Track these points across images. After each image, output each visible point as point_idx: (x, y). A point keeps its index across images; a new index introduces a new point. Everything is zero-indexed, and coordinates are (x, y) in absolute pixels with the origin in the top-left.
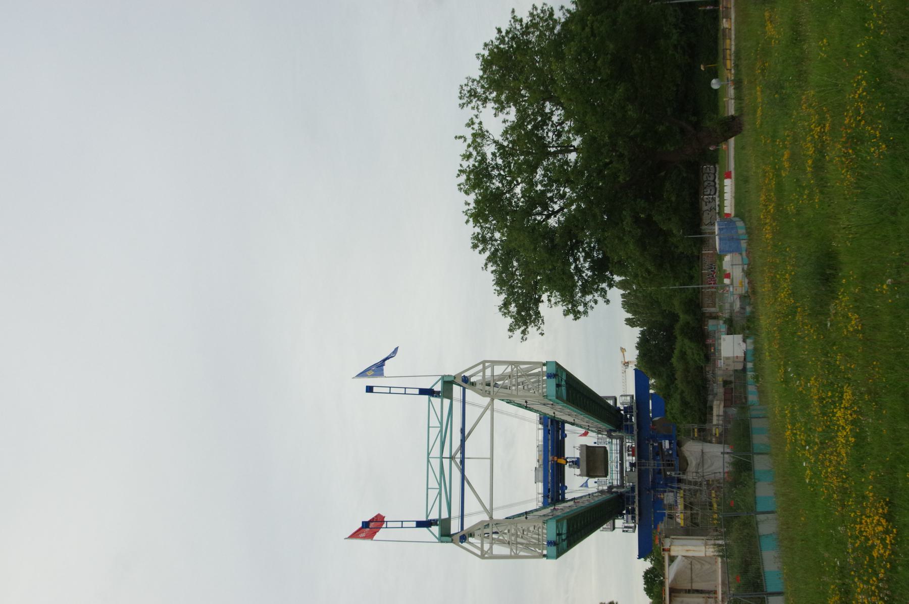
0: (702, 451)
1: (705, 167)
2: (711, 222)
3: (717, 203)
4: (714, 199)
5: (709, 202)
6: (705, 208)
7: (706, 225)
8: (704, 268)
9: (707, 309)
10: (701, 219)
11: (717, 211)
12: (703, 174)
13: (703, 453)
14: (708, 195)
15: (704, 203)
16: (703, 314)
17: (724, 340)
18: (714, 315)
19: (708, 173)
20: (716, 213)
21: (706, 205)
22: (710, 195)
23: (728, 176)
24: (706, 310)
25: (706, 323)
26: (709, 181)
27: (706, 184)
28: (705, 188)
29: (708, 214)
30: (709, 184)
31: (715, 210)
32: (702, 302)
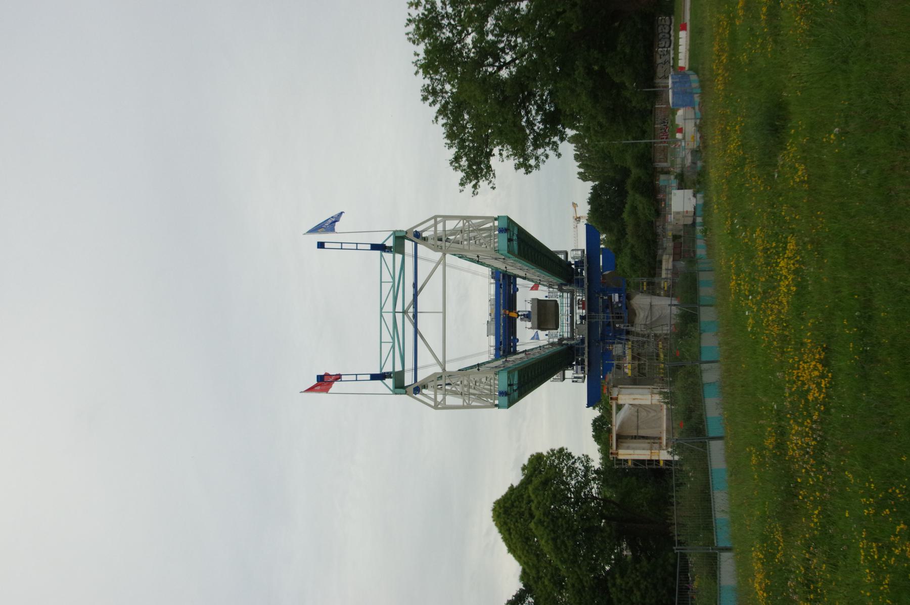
0: (651, 304)
1: (660, 18)
2: (665, 76)
3: (672, 56)
4: (668, 52)
5: (664, 55)
6: (659, 61)
7: (661, 78)
8: (657, 122)
9: (659, 164)
10: (655, 73)
11: (671, 64)
12: (658, 26)
13: (651, 305)
14: (662, 48)
15: (658, 56)
16: (655, 168)
17: (675, 194)
18: (665, 170)
19: (664, 25)
20: (670, 66)
21: (661, 58)
22: (664, 47)
23: (684, 28)
24: (658, 165)
25: (657, 178)
26: (665, 33)
27: (661, 36)
28: (660, 40)
29: (663, 67)
30: (664, 36)
31: (670, 63)
32: (654, 157)
